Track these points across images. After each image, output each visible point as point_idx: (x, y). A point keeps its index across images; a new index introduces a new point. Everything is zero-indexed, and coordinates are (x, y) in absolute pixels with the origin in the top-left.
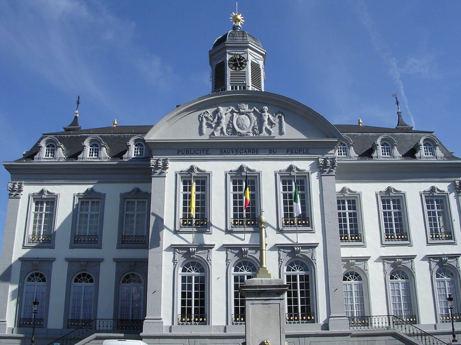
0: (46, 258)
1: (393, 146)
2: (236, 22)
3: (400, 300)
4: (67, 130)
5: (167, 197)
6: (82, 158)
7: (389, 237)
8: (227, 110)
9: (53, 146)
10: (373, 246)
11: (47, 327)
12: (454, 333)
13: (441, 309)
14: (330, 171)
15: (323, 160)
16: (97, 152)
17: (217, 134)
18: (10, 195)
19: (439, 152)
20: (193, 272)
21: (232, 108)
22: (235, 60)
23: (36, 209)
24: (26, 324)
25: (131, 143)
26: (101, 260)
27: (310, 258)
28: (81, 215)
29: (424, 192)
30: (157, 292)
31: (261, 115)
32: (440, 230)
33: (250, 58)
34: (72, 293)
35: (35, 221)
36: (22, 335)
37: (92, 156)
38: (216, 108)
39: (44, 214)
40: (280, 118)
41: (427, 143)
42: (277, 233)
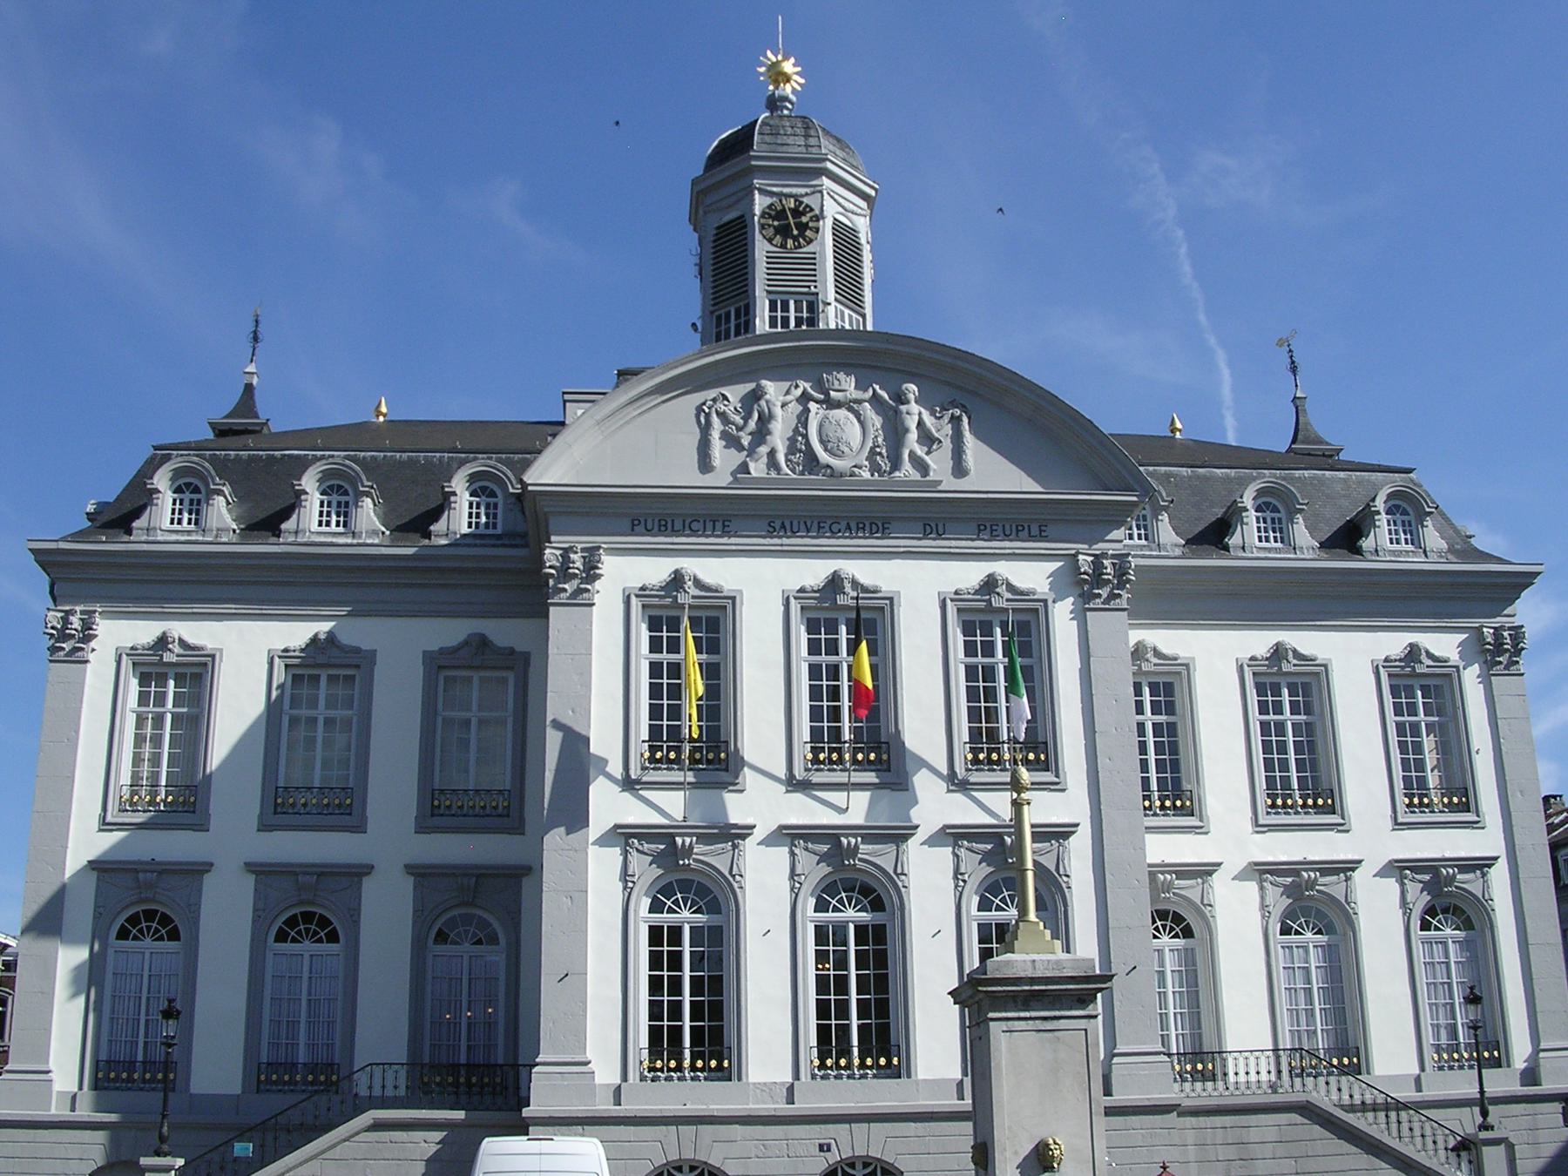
0: (180, 863)
1: (1292, 513)
2: (777, 83)
3: (1310, 1001)
4: (222, 432)
5: (597, 669)
6: (296, 533)
7: (1279, 802)
8: (788, 393)
9: (197, 490)
10: (1230, 831)
11: (188, 1085)
12: (1483, 1103)
13: (1436, 1027)
14: (1113, 596)
15: (1090, 559)
16: (345, 512)
17: (758, 469)
18: (54, 650)
19: (1432, 537)
20: (686, 914)
21: (804, 385)
22: (781, 215)
23: (143, 699)
24: (153, 1080)
25: (459, 485)
26: (366, 870)
27: (1053, 869)
28: (294, 721)
29: (1386, 660)
30: (574, 975)
31: (897, 412)
32: (1435, 780)
33: (831, 209)
34: (268, 978)
35: (139, 740)
36: (113, 1117)
37: (328, 524)
38: (752, 386)
39: (169, 717)
40: (956, 421)
41: (1397, 507)
42: (949, 791)
